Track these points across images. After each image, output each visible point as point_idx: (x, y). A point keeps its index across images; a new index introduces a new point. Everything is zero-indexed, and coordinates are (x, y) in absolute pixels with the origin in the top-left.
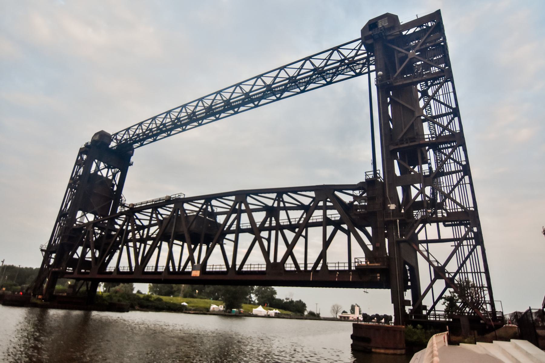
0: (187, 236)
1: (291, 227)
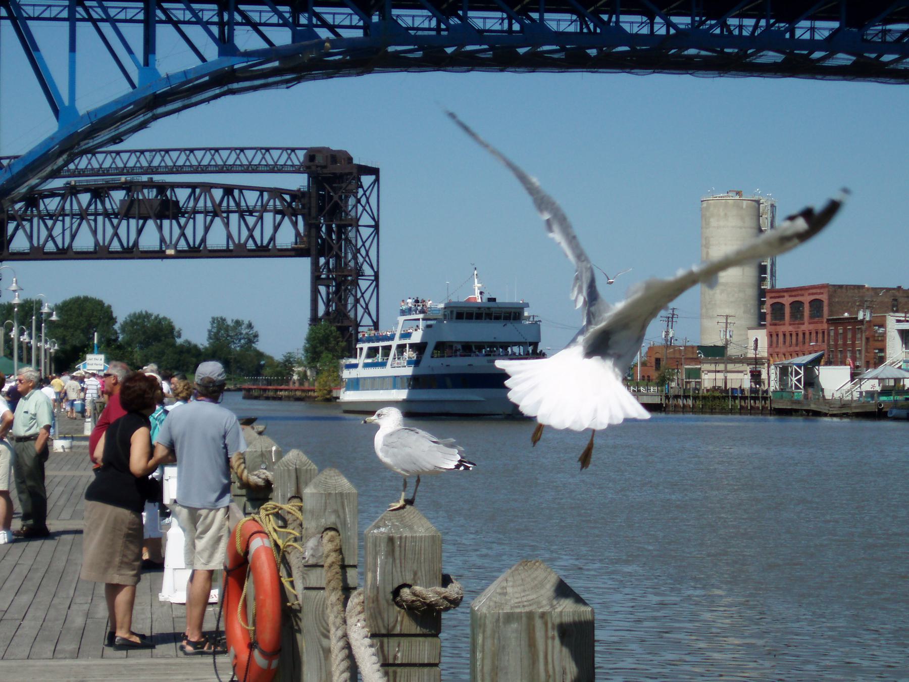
0: (152, 214)
1: (51, 216)
